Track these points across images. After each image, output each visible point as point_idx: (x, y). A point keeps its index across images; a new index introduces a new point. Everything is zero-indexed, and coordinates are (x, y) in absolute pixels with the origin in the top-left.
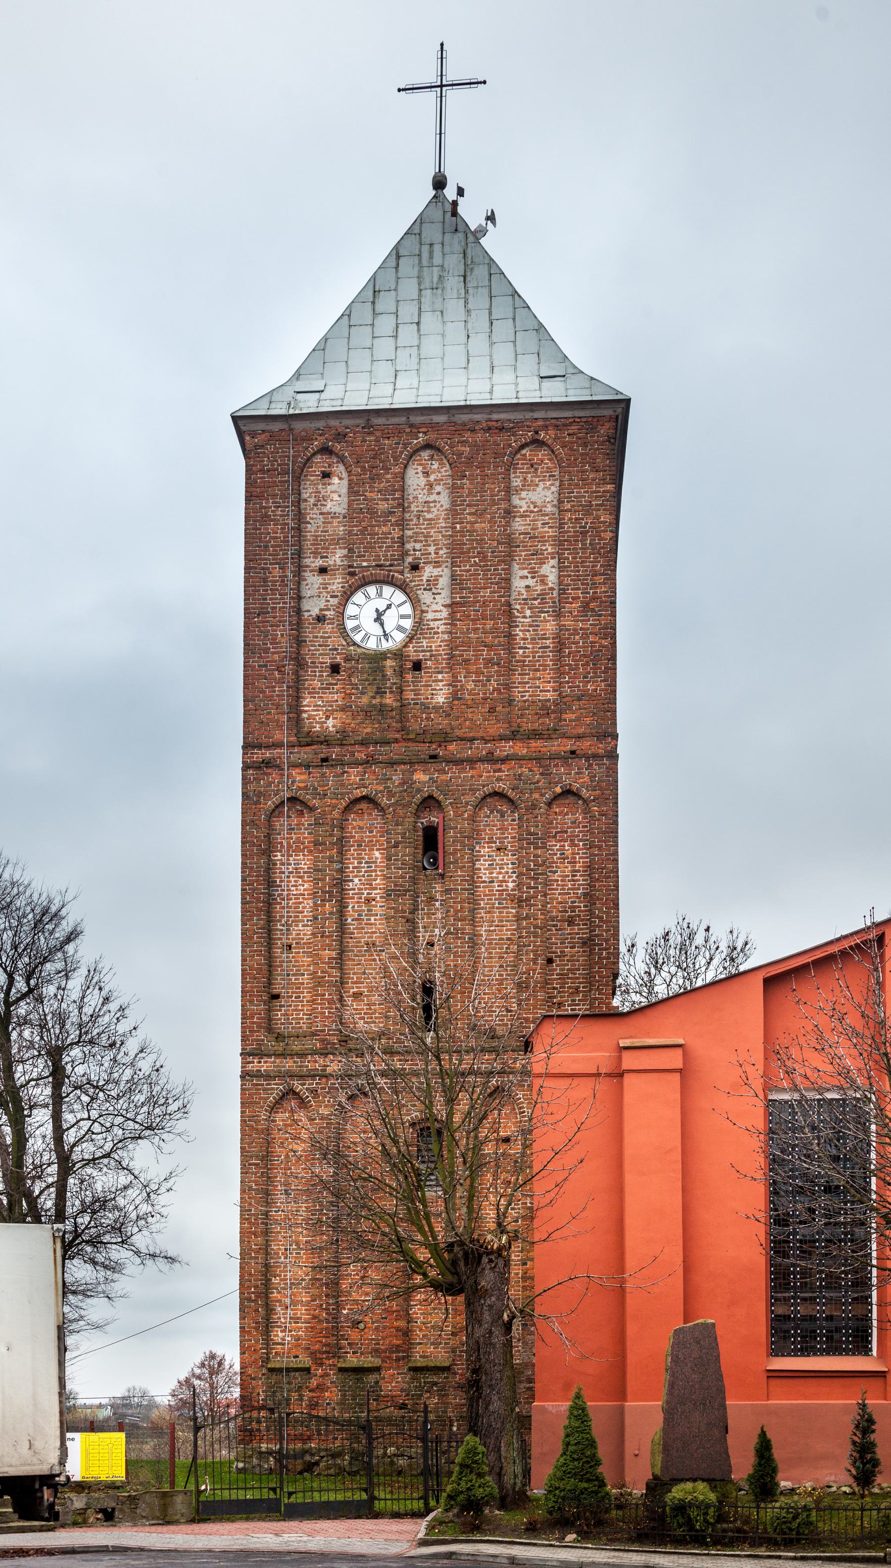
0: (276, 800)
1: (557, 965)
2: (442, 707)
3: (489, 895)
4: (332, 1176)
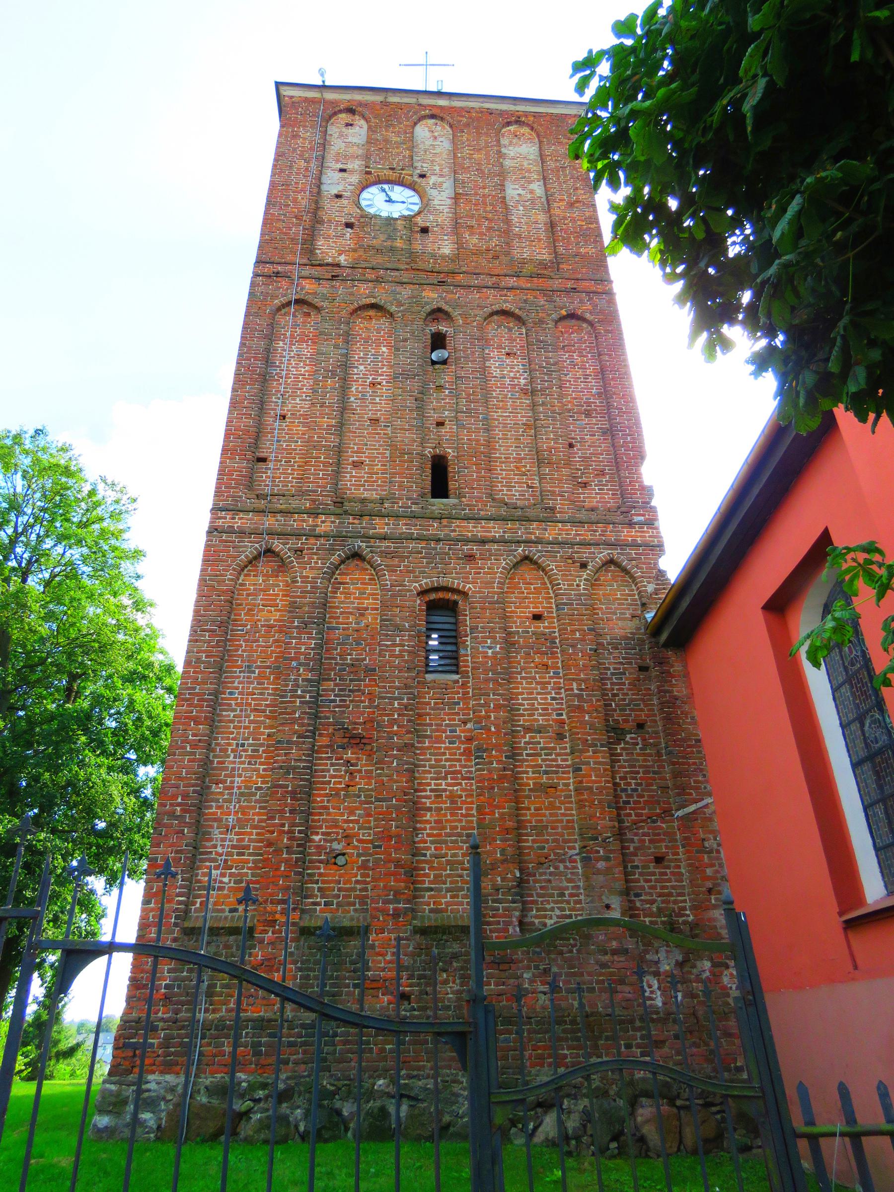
0: (284, 300)
1: (578, 450)
2: (448, 256)
3: (454, 737)
4: (313, 649)
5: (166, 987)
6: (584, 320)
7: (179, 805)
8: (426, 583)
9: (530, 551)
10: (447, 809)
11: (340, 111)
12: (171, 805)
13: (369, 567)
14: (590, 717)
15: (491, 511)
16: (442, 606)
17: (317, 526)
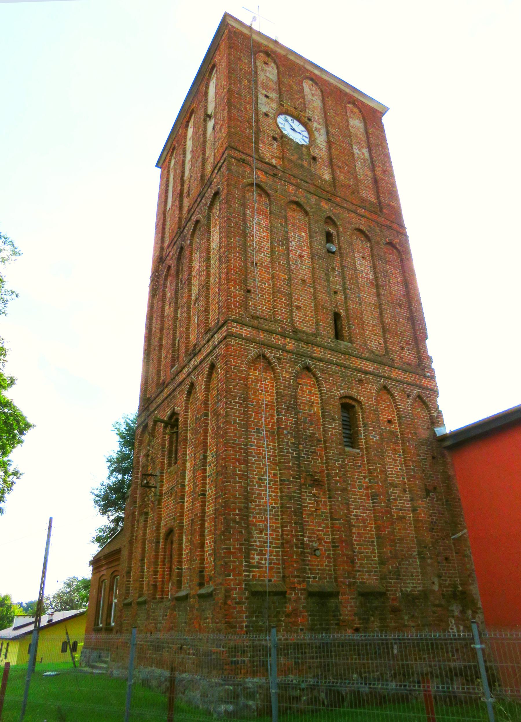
5: (246, 626)
6: (396, 248)
7: (237, 515)
8: (343, 393)
9: (386, 383)
10: (362, 526)
11: (261, 52)
12: (233, 514)
13: (312, 376)
14: (419, 482)
15: (366, 355)
16: (348, 407)
17: (286, 344)
